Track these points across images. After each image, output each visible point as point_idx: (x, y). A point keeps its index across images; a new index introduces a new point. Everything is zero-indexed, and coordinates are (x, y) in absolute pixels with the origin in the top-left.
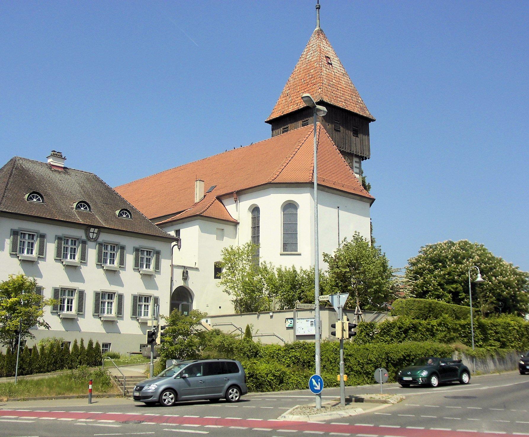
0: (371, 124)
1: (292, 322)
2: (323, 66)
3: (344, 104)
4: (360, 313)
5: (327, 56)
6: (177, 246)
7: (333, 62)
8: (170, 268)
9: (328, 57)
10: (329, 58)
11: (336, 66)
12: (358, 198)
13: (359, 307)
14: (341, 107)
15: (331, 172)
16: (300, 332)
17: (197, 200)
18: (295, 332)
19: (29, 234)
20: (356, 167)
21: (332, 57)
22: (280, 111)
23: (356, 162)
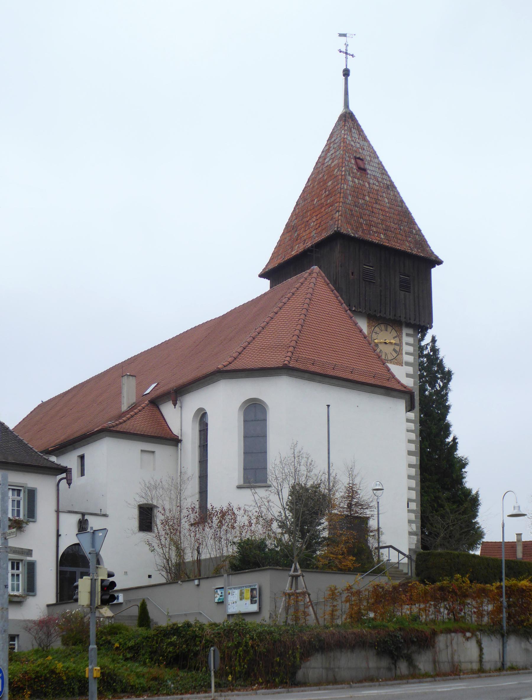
0: (435, 271)
1: (223, 594)
2: (347, 173)
3: (382, 236)
4: (299, 572)
5: (358, 156)
6: (65, 480)
7: (367, 167)
8: (54, 515)
9: (359, 158)
10: (362, 160)
11: (374, 173)
12: (382, 390)
13: (297, 564)
14: (374, 241)
15: (331, 349)
16: (232, 609)
17: (124, 408)
18: (226, 610)
19: (13, 489)
20: (407, 344)
21: (368, 158)
22: (279, 257)
23: (408, 335)
